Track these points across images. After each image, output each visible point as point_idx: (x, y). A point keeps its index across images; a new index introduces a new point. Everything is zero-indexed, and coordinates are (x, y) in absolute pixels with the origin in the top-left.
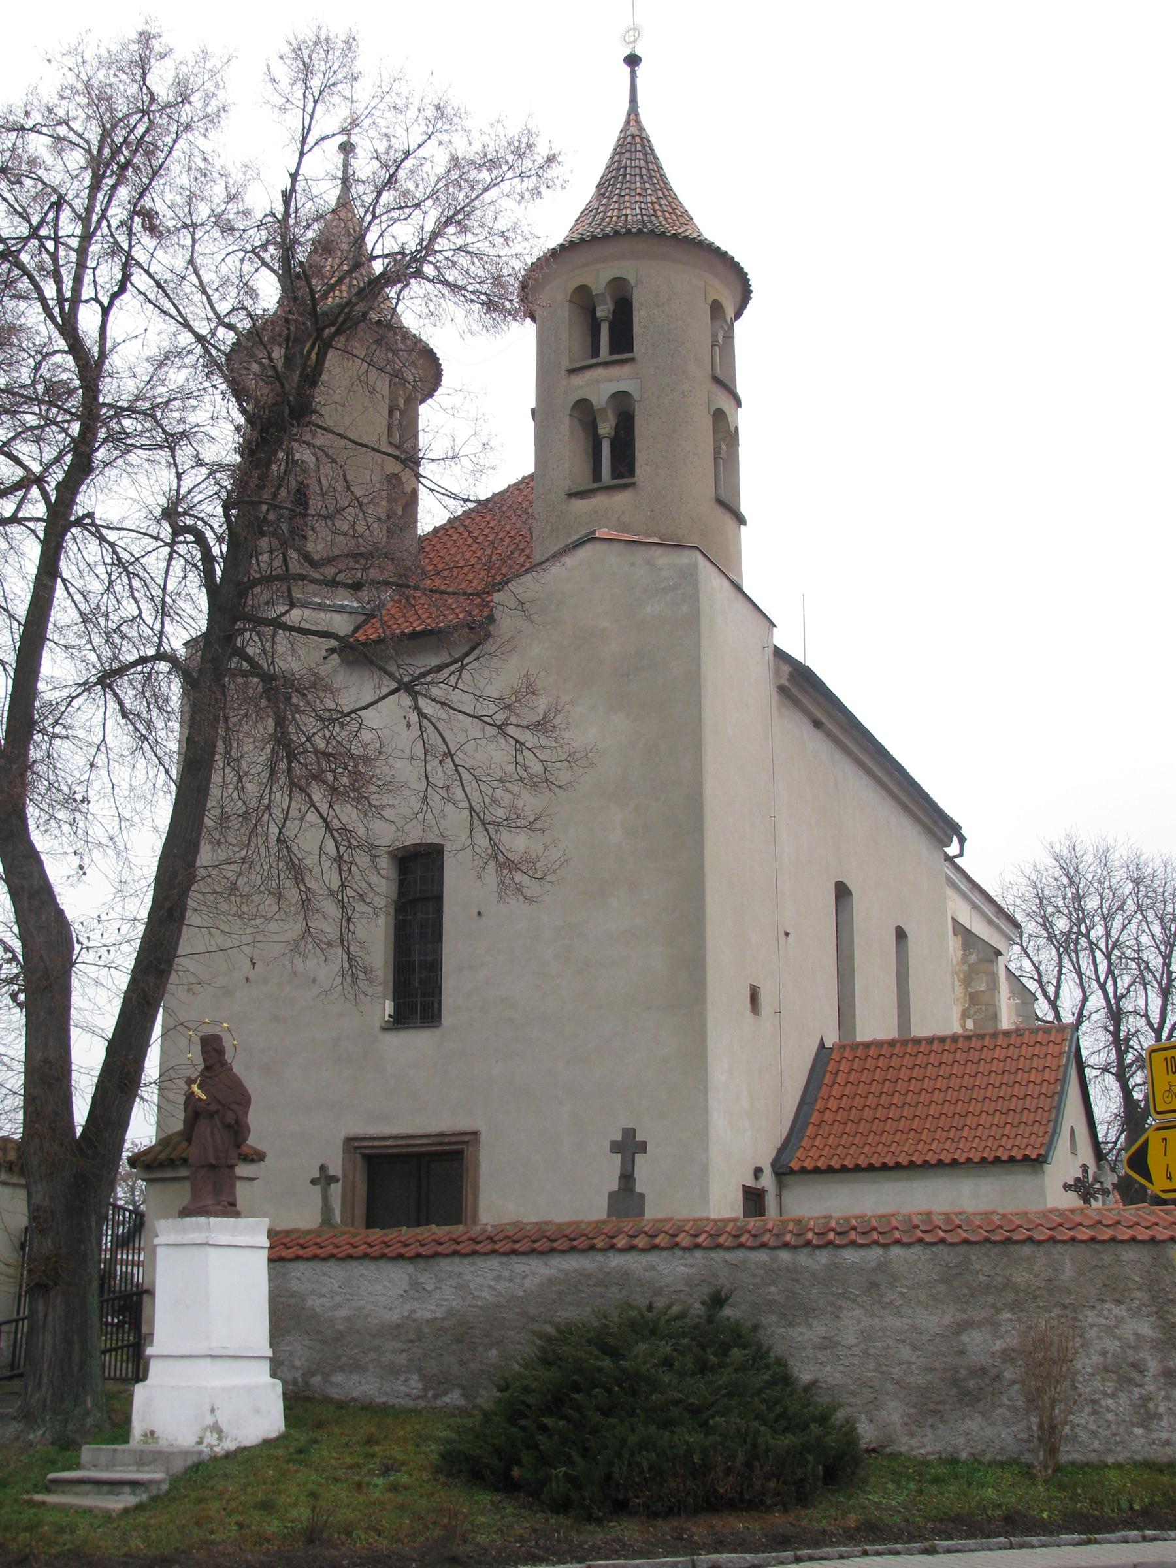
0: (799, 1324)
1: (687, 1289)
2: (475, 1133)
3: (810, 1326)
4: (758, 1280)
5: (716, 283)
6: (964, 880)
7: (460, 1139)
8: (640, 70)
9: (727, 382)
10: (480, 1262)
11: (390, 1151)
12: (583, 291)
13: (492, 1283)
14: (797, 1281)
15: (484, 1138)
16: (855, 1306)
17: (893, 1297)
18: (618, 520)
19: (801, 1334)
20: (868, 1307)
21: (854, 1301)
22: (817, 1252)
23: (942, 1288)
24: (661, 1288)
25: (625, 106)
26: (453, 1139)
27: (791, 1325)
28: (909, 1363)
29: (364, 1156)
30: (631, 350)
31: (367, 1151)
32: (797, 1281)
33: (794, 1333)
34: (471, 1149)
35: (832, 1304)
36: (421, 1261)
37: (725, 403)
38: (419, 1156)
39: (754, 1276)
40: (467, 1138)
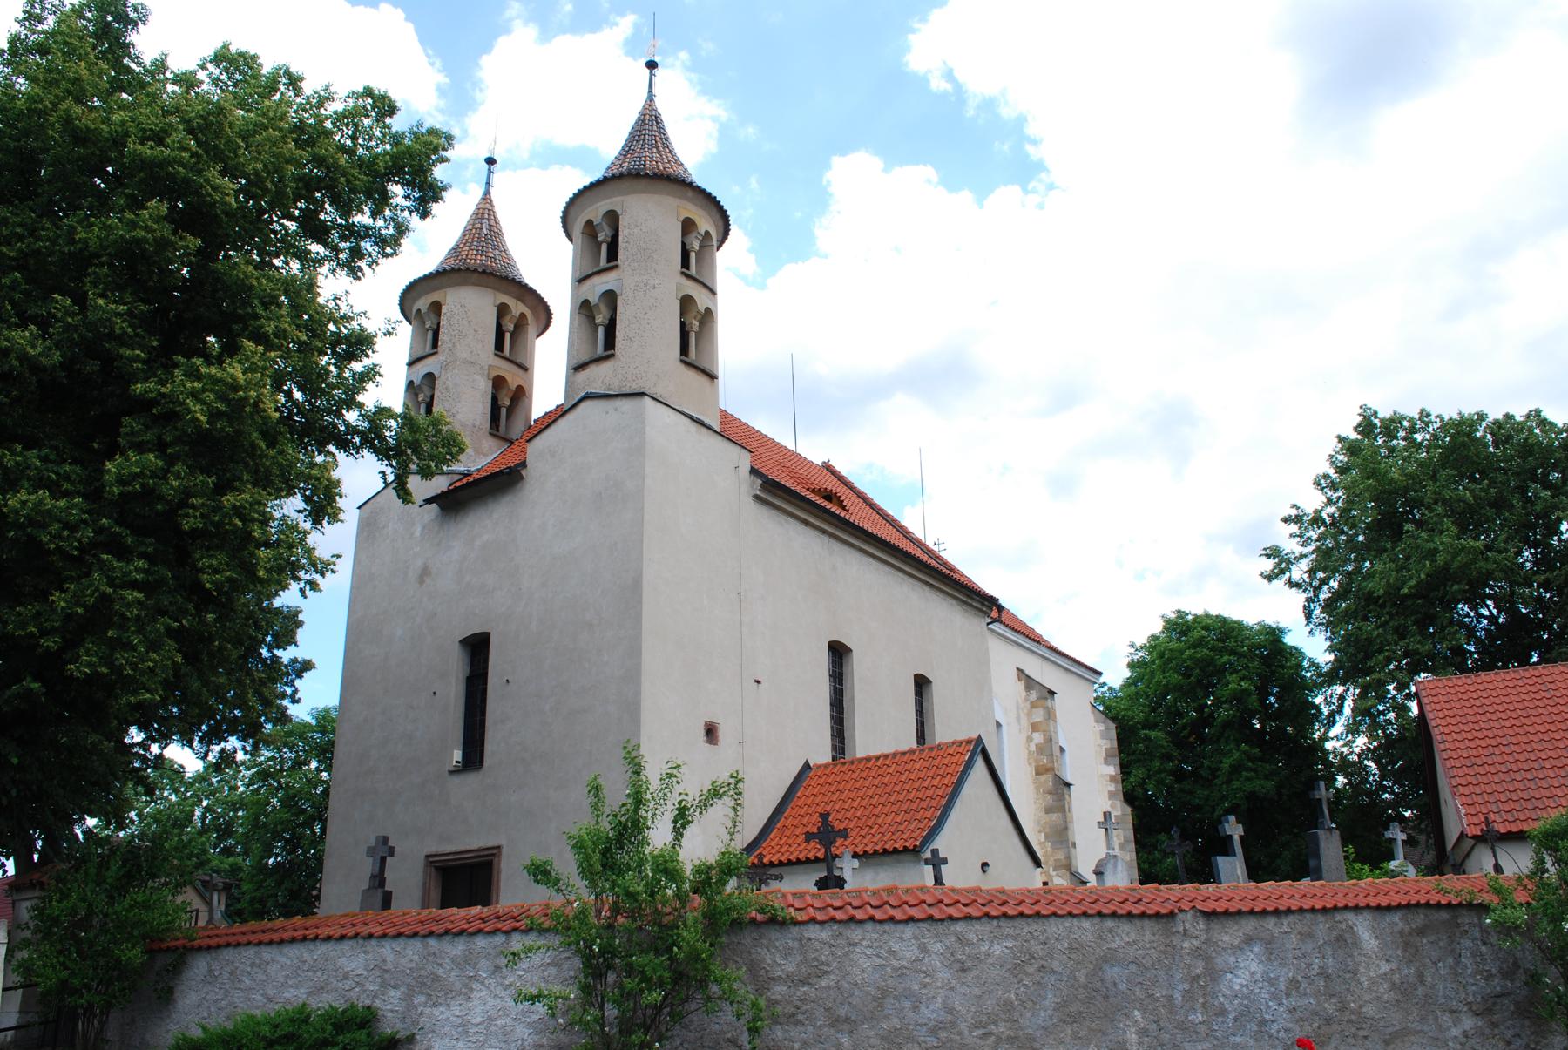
0: (441, 1004)
1: (365, 973)
2: (499, 847)
3: (448, 1006)
4: (413, 965)
5: (690, 206)
6: (1083, 670)
7: (490, 852)
8: (658, 72)
9: (709, 285)
10: (286, 949)
11: (450, 863)
12: (589, 223)
13: (249, 969)
14: (441, 965)
15: (504, 851)
16: (483, 988)
17: (512, 980)
18: (602, 382)
19: (442, 1013)
20: (492, 988)
21: (483, 983)
22: (456, 939)
23: (553, 971)
24: (348, 972)
25: (645, 95)
26: (486, 853)
27: (435, 1005)
28: (523, 1040)
29: (436, 868)
30: (617, 260)
31: (437, 865)
32: (441, 965)
33: (436, 1012)
34: (496, 859)
35: (466, 986)
36: (212, 951)
37: (702, 299)
38: (472, 866)
39: (412, 961)
40: (494, 852)
